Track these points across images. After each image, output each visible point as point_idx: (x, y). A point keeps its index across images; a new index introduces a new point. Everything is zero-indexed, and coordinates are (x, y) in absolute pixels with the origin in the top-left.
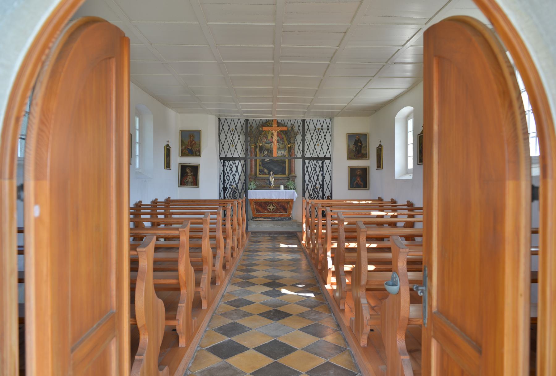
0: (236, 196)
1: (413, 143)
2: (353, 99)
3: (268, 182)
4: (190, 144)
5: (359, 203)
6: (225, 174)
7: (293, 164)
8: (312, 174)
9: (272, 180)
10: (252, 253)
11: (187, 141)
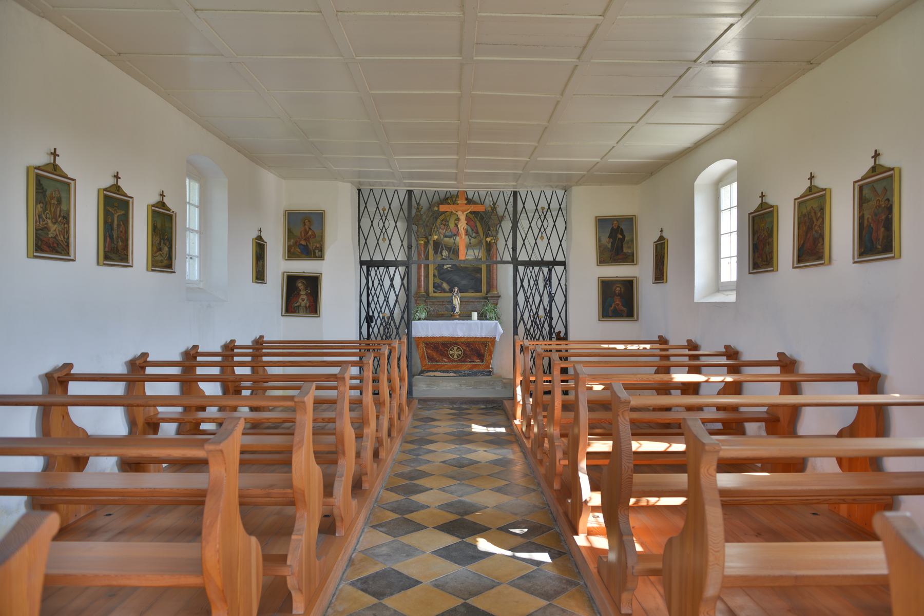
0: (390, 334)
1: (736, 230)
2: (614, 147)
3: (449, 307)
4: (305, 236)
5: (625, 349)
6: (371, 293)
7: (495, 274)
8: (531, 290)
9: (457, 302)
10: (418, 447)
11: (298, 231)
